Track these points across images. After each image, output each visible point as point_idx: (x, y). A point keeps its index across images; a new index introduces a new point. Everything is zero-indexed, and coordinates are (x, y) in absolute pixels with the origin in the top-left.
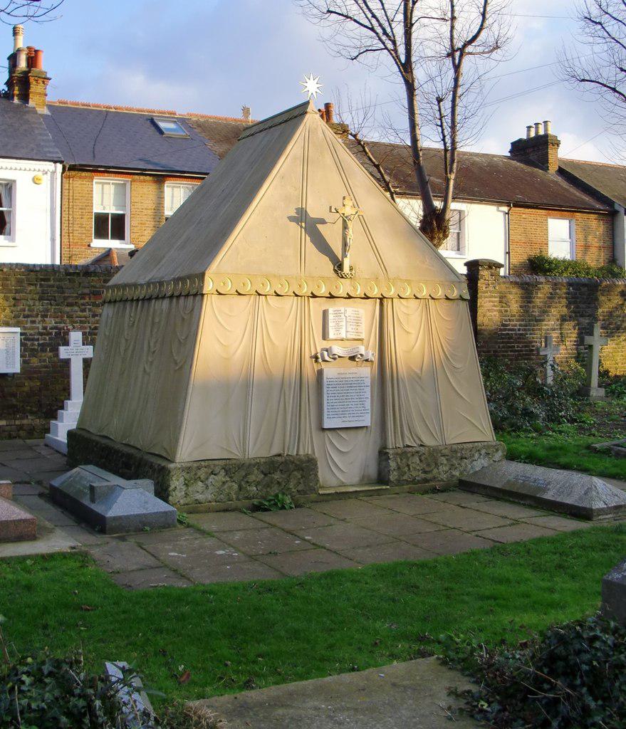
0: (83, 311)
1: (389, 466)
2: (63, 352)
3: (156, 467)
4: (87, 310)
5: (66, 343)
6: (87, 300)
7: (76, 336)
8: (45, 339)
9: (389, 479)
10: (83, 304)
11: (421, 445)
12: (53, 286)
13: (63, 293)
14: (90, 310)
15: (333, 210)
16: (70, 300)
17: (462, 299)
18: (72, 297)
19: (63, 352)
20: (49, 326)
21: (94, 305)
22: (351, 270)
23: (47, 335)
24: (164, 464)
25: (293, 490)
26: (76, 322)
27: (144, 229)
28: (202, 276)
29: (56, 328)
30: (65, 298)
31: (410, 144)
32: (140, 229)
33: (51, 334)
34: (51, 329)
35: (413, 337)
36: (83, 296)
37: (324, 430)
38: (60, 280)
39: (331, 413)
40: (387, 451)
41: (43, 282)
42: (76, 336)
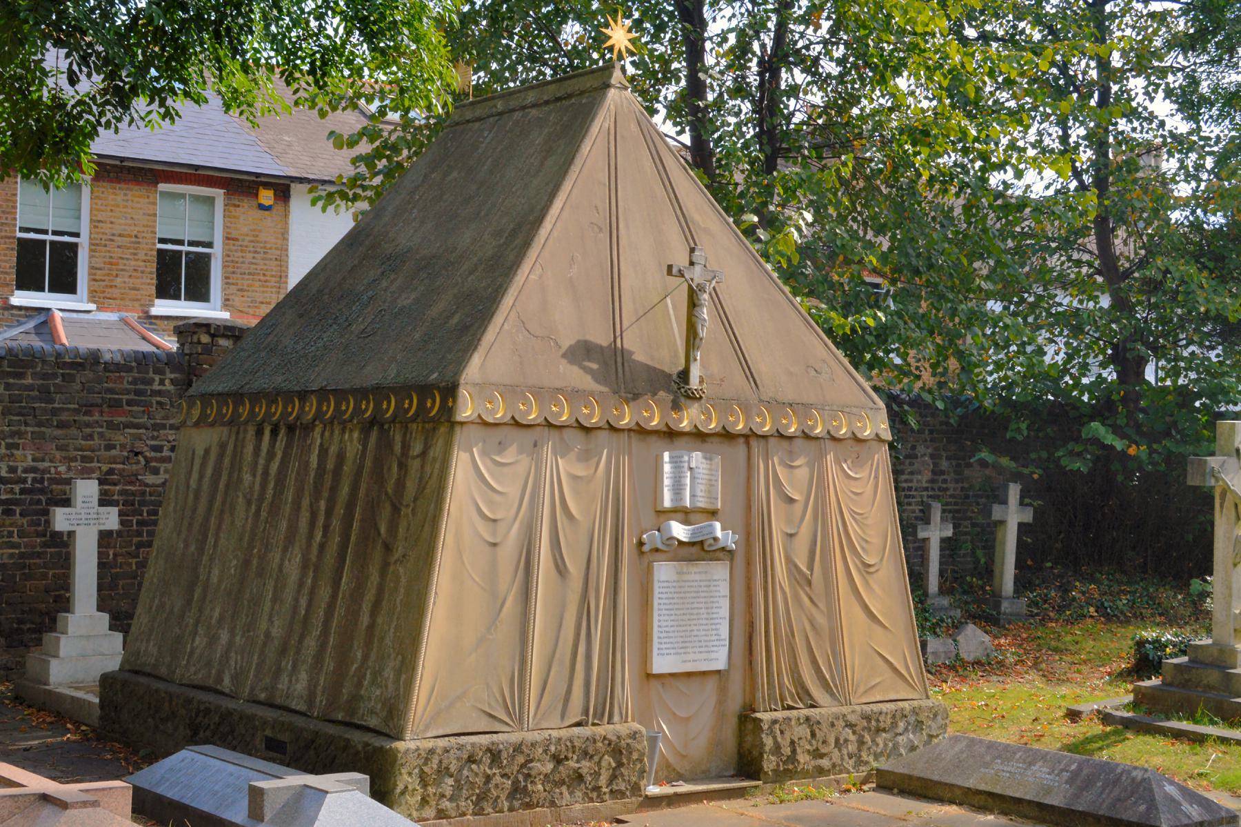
0: (90, 437)
1: (762, 745)
2: (61, 519)
3: (360, 747)
4: (96, 437)
5: (66, 502)
6: (97, 417)
7: (87, 489)
8: (12, 491)
9: (761, 768)
10: (88, 425)
11: (812, 706)
12: (30, 388)
13: (52, 401)
14: (101, 435)
15: (675, 271)
16: (64, 417)
17: (878, 438)
18: (68, 409)
19: (61, 519)
20: (21, 466)
21: (111, 426)
22: (701, 382)
23: (16, 483)
24: (377, 742)
25: (604, 790)
26: (74, 459)
27: (114, 273)
28: (450, 391)
29: (34, 470)
30: (55, 412)
31: (688, 143)
32: (108, 275)
33: (24, 481)
34: (25, 471)
35: (798, 508)
36: (87, 408)
37: (649, 676)
38: (45, 376)
39: (664, 646)
40: (758, 715)
41: (11, 381)
42: (87, 489)
